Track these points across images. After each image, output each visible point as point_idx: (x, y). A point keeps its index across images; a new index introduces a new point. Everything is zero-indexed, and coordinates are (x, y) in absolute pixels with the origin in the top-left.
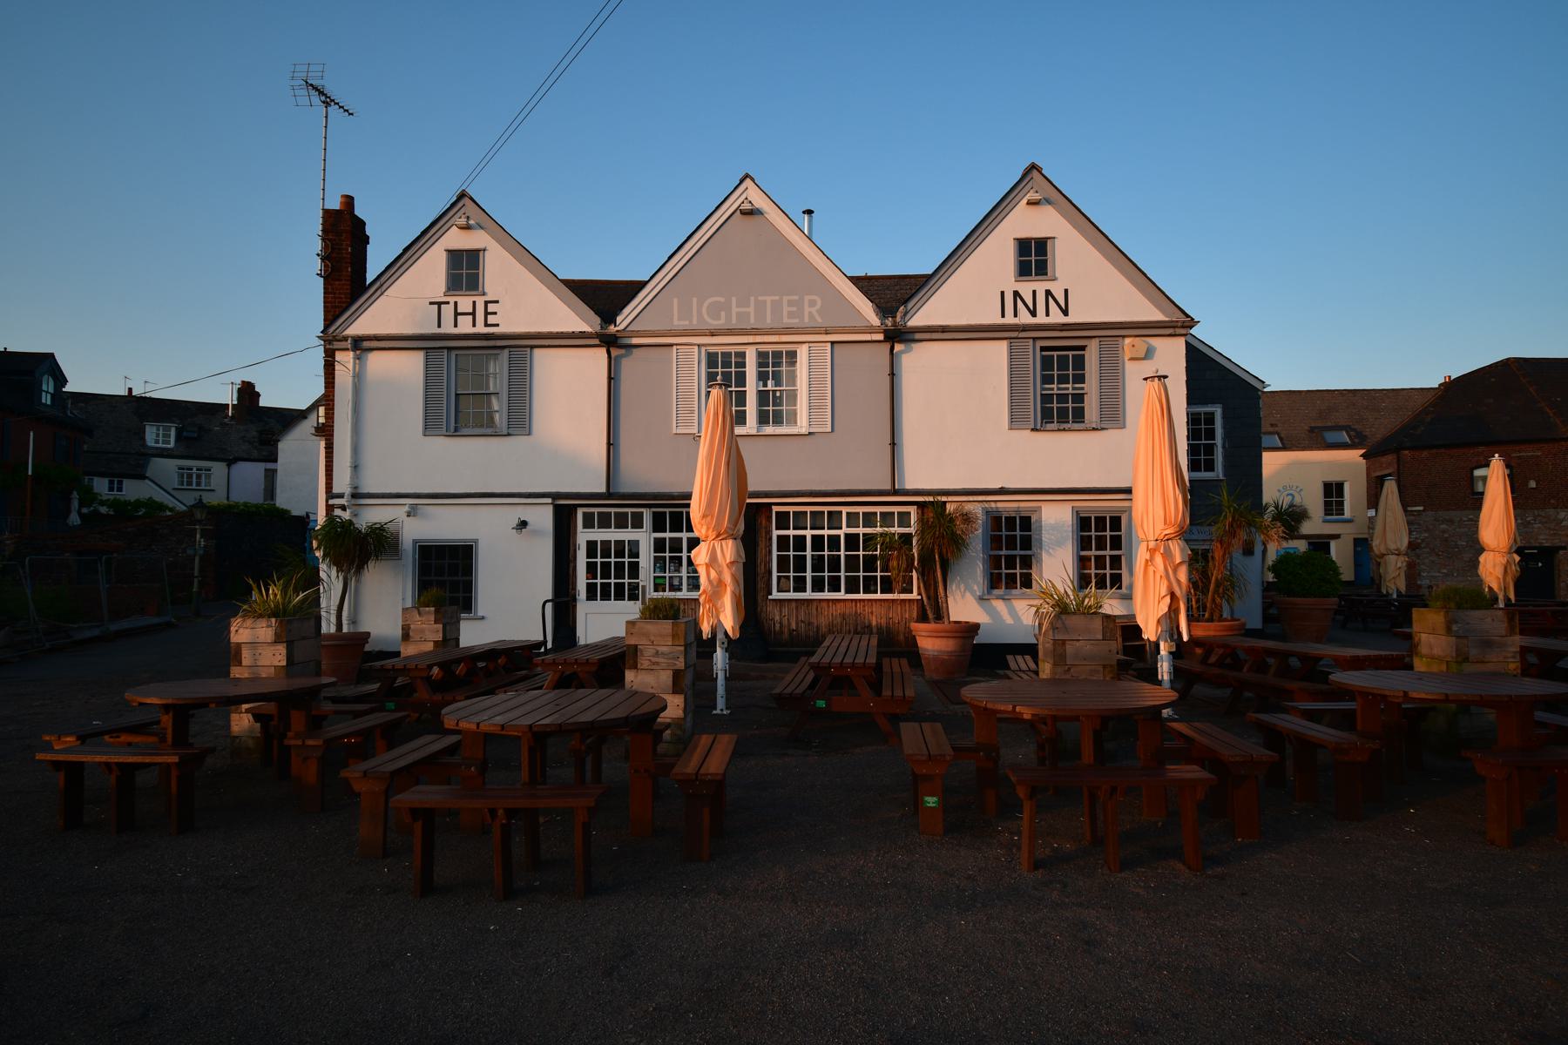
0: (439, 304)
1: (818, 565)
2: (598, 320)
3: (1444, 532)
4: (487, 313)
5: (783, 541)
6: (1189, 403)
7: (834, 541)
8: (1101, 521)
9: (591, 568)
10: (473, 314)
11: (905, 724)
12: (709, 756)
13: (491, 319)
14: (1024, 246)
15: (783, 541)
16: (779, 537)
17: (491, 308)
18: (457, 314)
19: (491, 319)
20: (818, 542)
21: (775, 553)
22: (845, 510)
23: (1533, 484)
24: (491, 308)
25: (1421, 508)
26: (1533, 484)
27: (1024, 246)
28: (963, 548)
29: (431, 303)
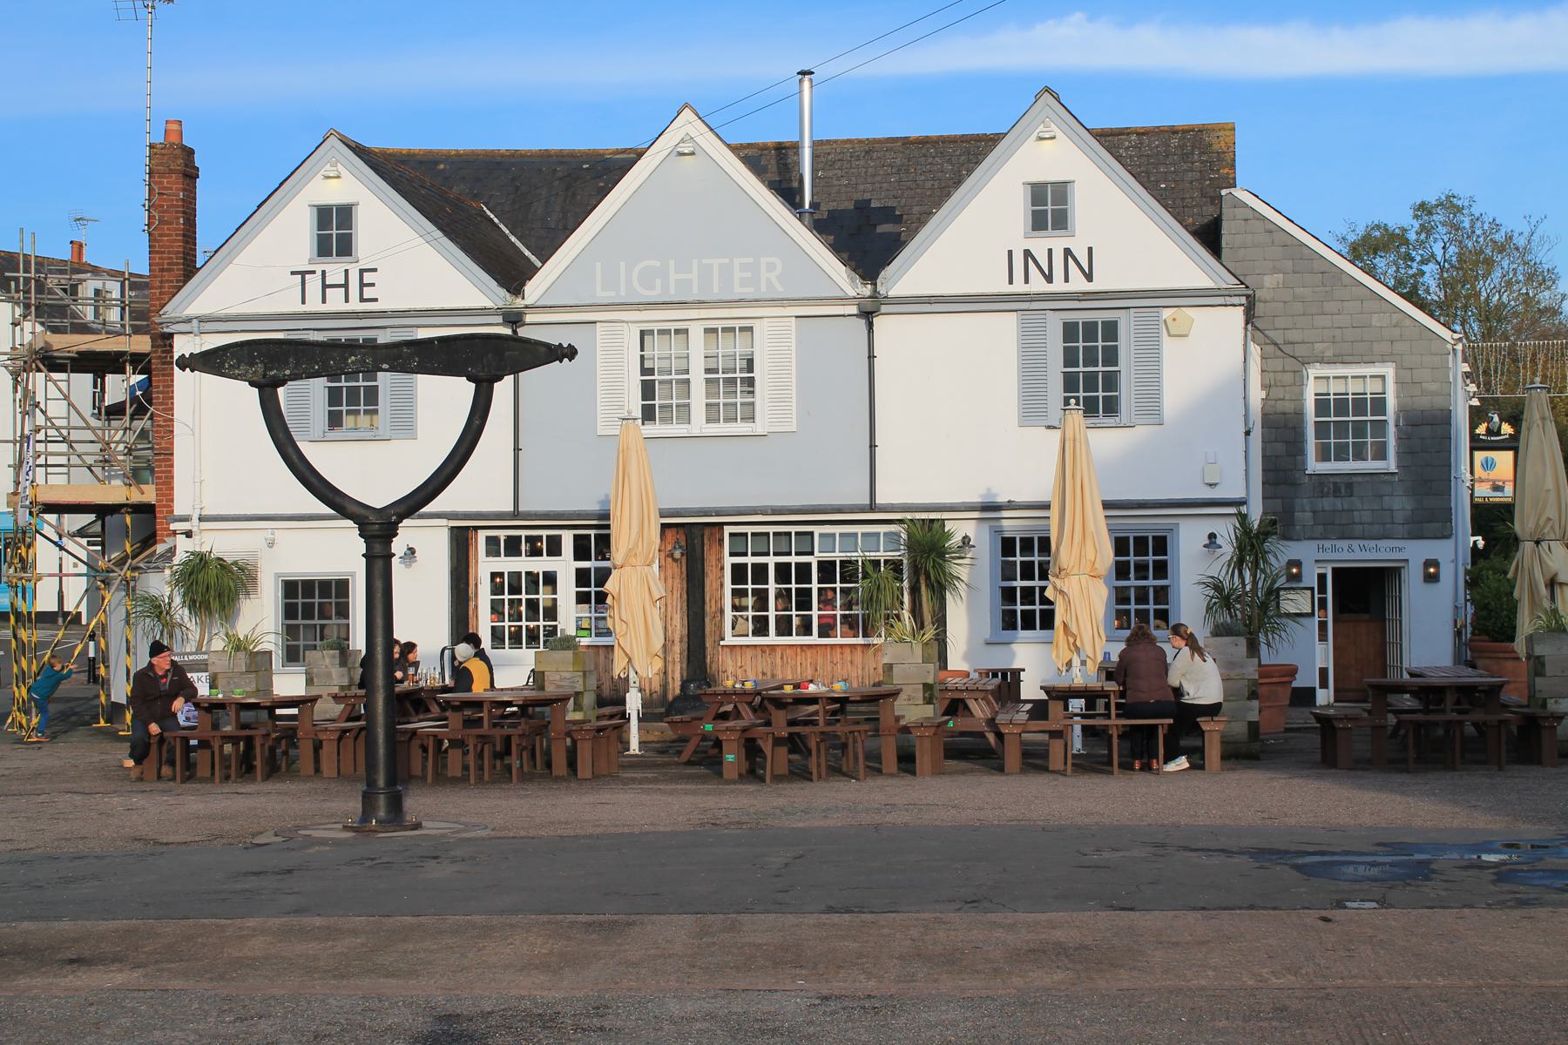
0: (303, 274)
4: (362, 285)
7: (804, 572)
8: (1141, 543)
10: (346, 286)
13: (368, 292)
16: (734, 566)
17: (368, 278)
18: (325, 286)
19: (368, 292)
21: (728, 586)
24: (368, 278)
29: (293, 273)
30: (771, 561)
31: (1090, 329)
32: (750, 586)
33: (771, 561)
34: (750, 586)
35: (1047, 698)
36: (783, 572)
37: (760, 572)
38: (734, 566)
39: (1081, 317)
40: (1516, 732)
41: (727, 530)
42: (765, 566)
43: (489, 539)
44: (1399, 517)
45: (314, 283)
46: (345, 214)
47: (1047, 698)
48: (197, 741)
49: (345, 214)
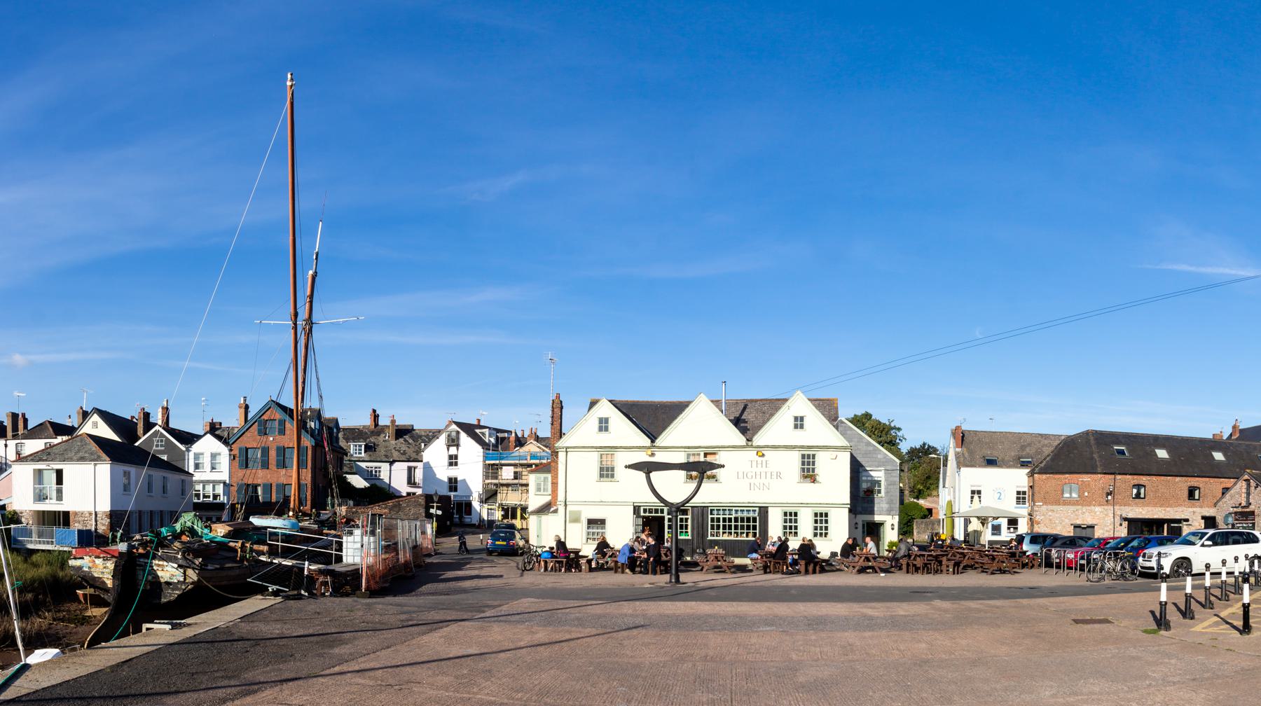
1: (724, 527)
2: (649, 441)
3: (1050, 516)
5: (712, 520)
6: (63, 512)
7: (730, 520)
8: (821, 515)
9: (686, 526)
11: (1193, 569)
12: (541, 643)
14: (601, 420)
15: (712, 520)
16: (711, 518)
20: (724, 520)
21: (710, 523)
22: (734, 509)
23: (1086, 494)
25: (1041, 504)
26: (1086, 494)
27: (601, 420)
28: (71, 581)
30: (721, 517)
31: (809, 456)
32: (751, 531)
33: (721, 517)
34: (751, 531)
35: (29, 429)
36: (724, 520)
37: (718, 520)
38: (711, 518)
39: (806, 453)
40: (117, 438)
41: (710, 508)
42: (719, 518)
43: (547, 491)
44: (885, 509)
45: (754, 464)
46: (607, 420)
47: (29, 429)
48: (250, 520)
49: (607, 420)
